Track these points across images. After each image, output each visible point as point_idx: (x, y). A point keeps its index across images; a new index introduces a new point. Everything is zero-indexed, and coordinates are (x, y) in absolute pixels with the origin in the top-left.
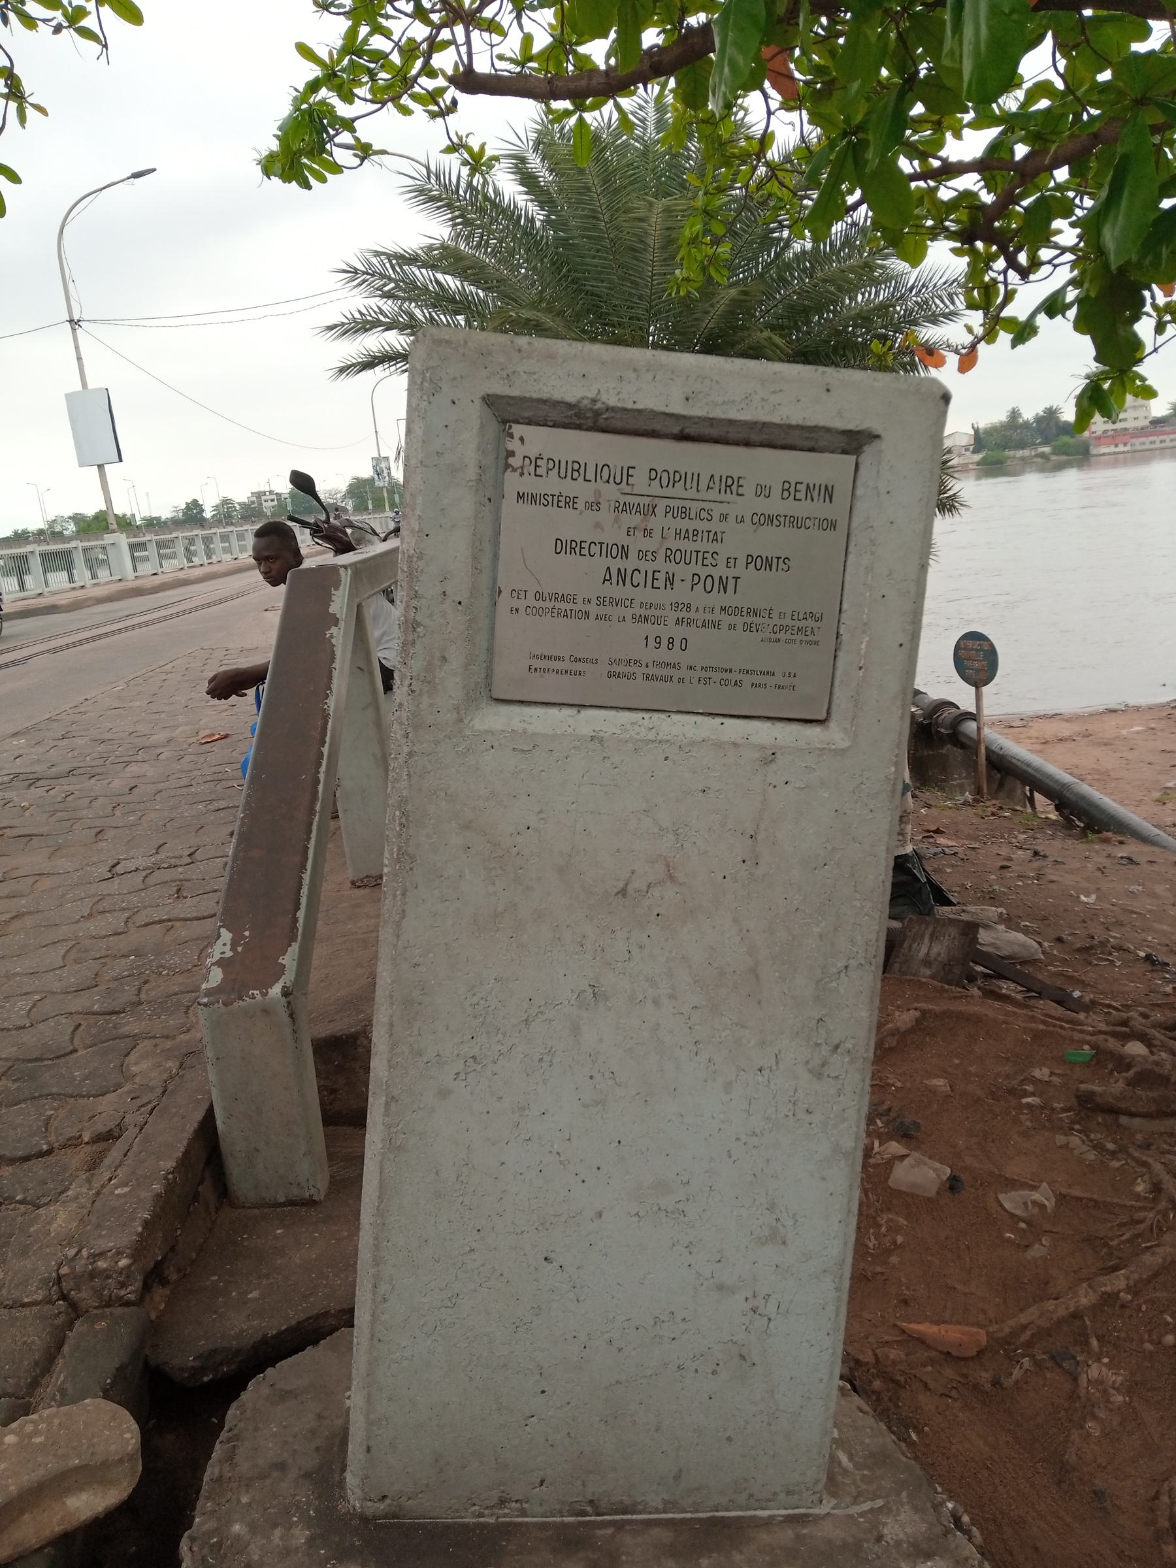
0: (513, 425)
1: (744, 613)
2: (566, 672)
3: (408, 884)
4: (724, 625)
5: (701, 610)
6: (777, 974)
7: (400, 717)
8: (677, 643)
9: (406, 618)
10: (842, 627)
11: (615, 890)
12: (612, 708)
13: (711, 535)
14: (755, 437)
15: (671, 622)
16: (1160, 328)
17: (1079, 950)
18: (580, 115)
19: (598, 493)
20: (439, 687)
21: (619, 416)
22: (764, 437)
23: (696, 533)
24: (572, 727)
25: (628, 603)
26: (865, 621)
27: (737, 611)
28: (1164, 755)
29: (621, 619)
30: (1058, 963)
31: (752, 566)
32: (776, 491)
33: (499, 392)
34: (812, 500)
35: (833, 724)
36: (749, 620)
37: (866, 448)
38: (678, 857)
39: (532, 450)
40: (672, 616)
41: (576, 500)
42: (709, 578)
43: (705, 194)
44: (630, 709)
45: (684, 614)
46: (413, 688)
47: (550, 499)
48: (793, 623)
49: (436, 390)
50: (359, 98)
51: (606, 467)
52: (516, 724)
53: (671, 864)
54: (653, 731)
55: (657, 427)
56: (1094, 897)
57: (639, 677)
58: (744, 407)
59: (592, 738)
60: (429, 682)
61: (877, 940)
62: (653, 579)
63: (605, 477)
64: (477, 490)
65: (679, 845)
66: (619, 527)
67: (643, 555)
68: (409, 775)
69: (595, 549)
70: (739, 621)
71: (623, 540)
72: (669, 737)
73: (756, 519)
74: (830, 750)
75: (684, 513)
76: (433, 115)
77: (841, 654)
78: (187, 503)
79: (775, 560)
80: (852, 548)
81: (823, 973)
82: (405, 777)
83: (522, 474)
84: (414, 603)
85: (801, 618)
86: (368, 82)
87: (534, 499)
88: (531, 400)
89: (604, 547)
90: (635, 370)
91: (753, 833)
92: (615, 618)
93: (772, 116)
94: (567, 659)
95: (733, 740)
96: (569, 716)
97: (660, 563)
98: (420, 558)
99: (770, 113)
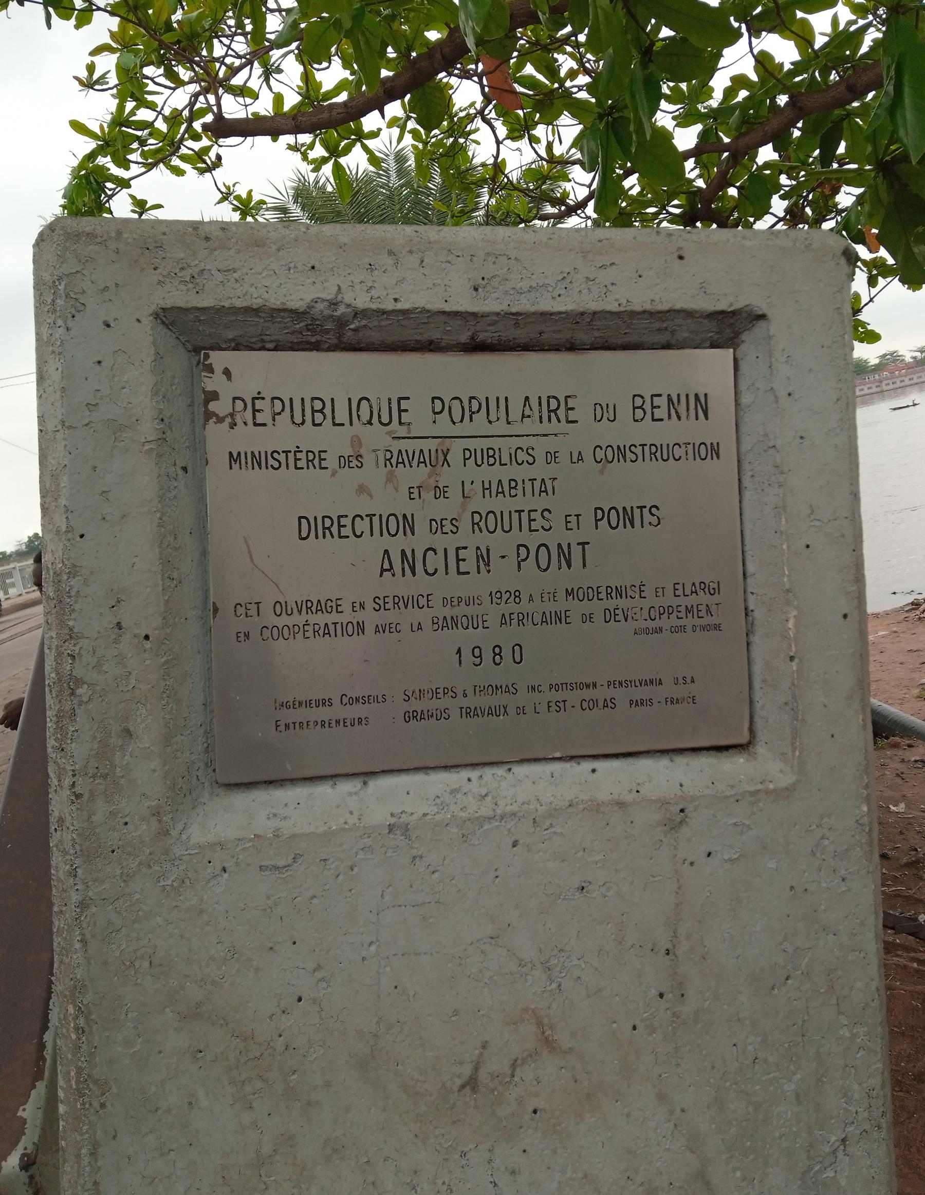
0: (211, 353)
1: (603, 595)
2: (338, 722)
3: (99, 1134)
4: (575, 617)
5: (537, 598)
6: (738, 1174)
7: (61, 842)
8: (507, 653)
9: (58, 674)
10: (752, 600)
11: (459, 1082)
12: (417, 769)
13: (537, 484)
14: (582, 336)
15: (493, 619)
16: (872, 282)
17: (907, 865)
18: (335, 160)
19: (356, 441)
20: (123, 781)
21: (376, 323)
22: (596, 334)
23: (513, 484)
24: (356, 814)
25: (423, 602)
26: (787, 586)
27: (592, 593)
28: (911, 654)
29: (415, 628)
30: (890, 882)
31: (603, 523)
32: (625, 411)
33: (181, 304)
34: (679, 418)
35: (760, 749)
36: (611, 604)
37: (744, 337)
38: (554, 1006)
39: (246, 386)
40: (494, 613)
41: (323, 455)
42: (543, 549)
43: (452, 217)
44: (446, 768)
45: (512, 607)
46: (78, 789)
47: (282, 458)
48: (677, 601)
49: (77, 308)
50: (133, 162)
51: (364, 402)
52: (263, 824)
53: (546, 1020)
54: (489, 799)
55: (435, 335)
56: (902, 805)
57: (455, 713)
58: (563, 292)
59: (391, 828)
60: (105, 777)
61: (883, 1087)
62: (458, 560)
63: (365, 417)
64: (160, 456)
65: (554, 986)
66: (396, 490)
67: (437, 525)
68: (84, 941)
69: (362, 526)
70: (597, 607)
71: (404, 507)
72: (515, 808)
73: (600, 454)
74: (768, 792)
75: (491, 456)
76: (202, 172)
77: (756, 639)
78: (29, 537)
79: (637, 512)
80: (747, 481)
81: (809, 1158)
82: (78, 946)
83: (233, 425)
84: (69, 647)
85: (688, 592)
86: (138, 148)
87: (257, 460)
88: (235, 310)
89: (376, 520)
90: (391, 253)
91: (670, 946)
92: (405, 628)
93: (501, 145)
94: (336, 701)
95: (615, 796)
96: (350, 794)
97: (465, 536)
98: (73, 573)
99: (498, 143)
